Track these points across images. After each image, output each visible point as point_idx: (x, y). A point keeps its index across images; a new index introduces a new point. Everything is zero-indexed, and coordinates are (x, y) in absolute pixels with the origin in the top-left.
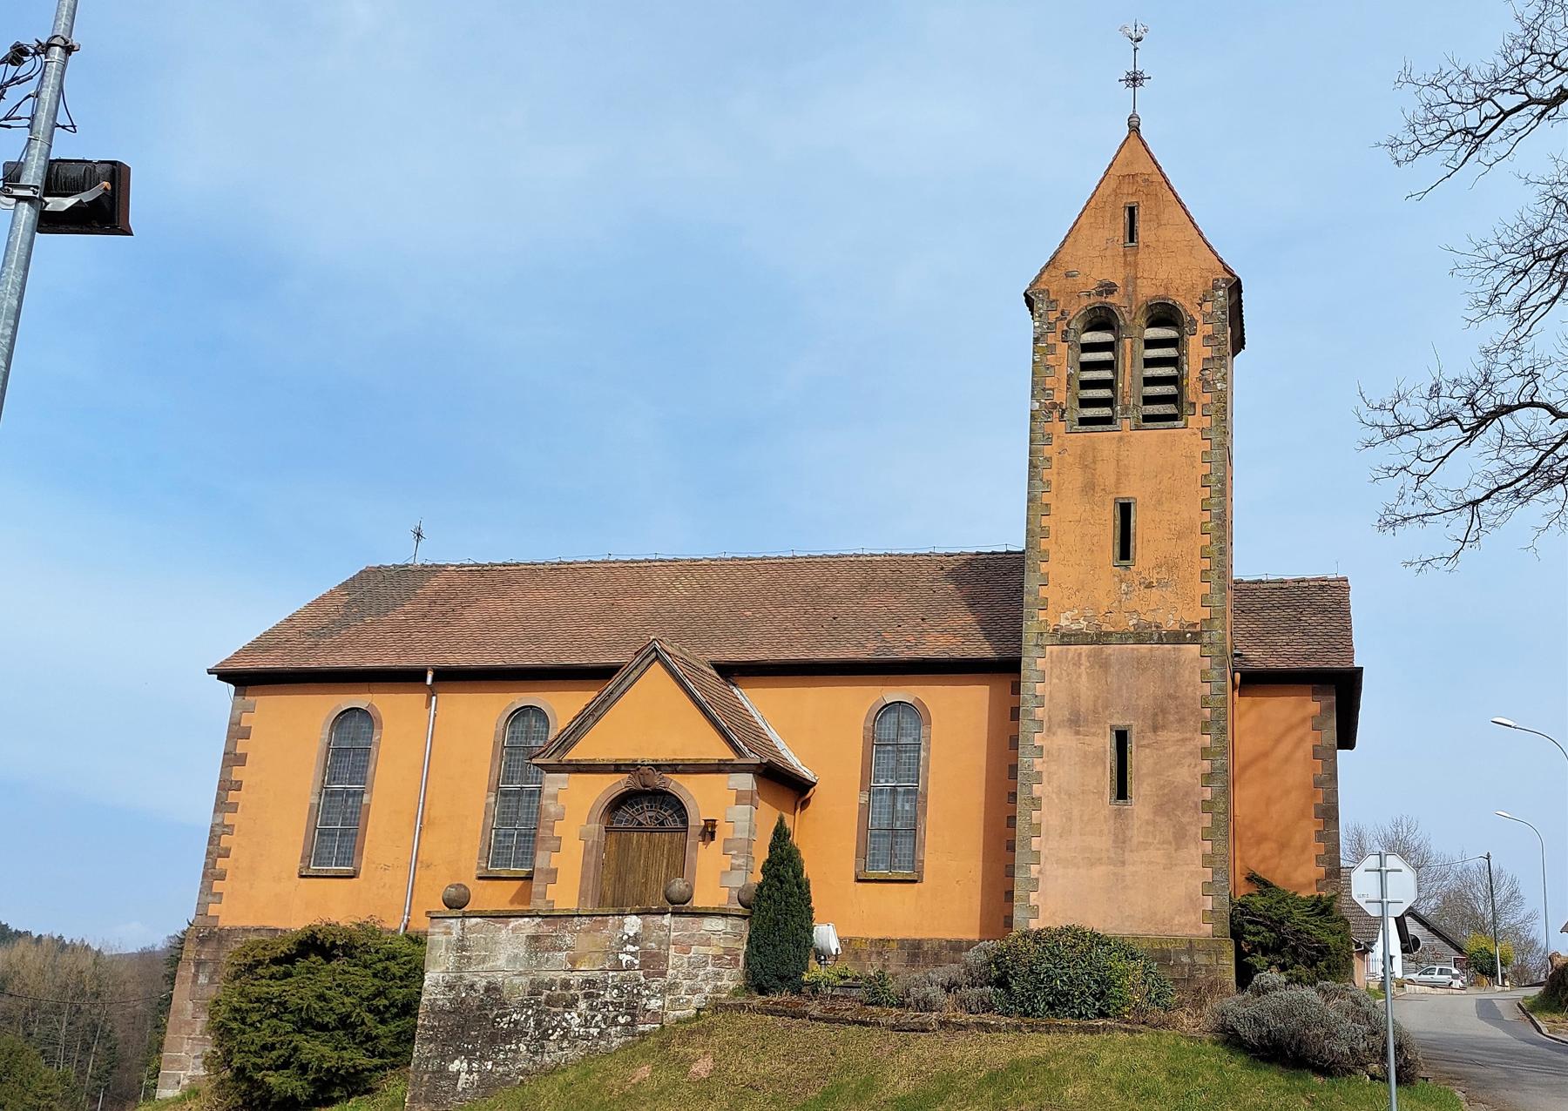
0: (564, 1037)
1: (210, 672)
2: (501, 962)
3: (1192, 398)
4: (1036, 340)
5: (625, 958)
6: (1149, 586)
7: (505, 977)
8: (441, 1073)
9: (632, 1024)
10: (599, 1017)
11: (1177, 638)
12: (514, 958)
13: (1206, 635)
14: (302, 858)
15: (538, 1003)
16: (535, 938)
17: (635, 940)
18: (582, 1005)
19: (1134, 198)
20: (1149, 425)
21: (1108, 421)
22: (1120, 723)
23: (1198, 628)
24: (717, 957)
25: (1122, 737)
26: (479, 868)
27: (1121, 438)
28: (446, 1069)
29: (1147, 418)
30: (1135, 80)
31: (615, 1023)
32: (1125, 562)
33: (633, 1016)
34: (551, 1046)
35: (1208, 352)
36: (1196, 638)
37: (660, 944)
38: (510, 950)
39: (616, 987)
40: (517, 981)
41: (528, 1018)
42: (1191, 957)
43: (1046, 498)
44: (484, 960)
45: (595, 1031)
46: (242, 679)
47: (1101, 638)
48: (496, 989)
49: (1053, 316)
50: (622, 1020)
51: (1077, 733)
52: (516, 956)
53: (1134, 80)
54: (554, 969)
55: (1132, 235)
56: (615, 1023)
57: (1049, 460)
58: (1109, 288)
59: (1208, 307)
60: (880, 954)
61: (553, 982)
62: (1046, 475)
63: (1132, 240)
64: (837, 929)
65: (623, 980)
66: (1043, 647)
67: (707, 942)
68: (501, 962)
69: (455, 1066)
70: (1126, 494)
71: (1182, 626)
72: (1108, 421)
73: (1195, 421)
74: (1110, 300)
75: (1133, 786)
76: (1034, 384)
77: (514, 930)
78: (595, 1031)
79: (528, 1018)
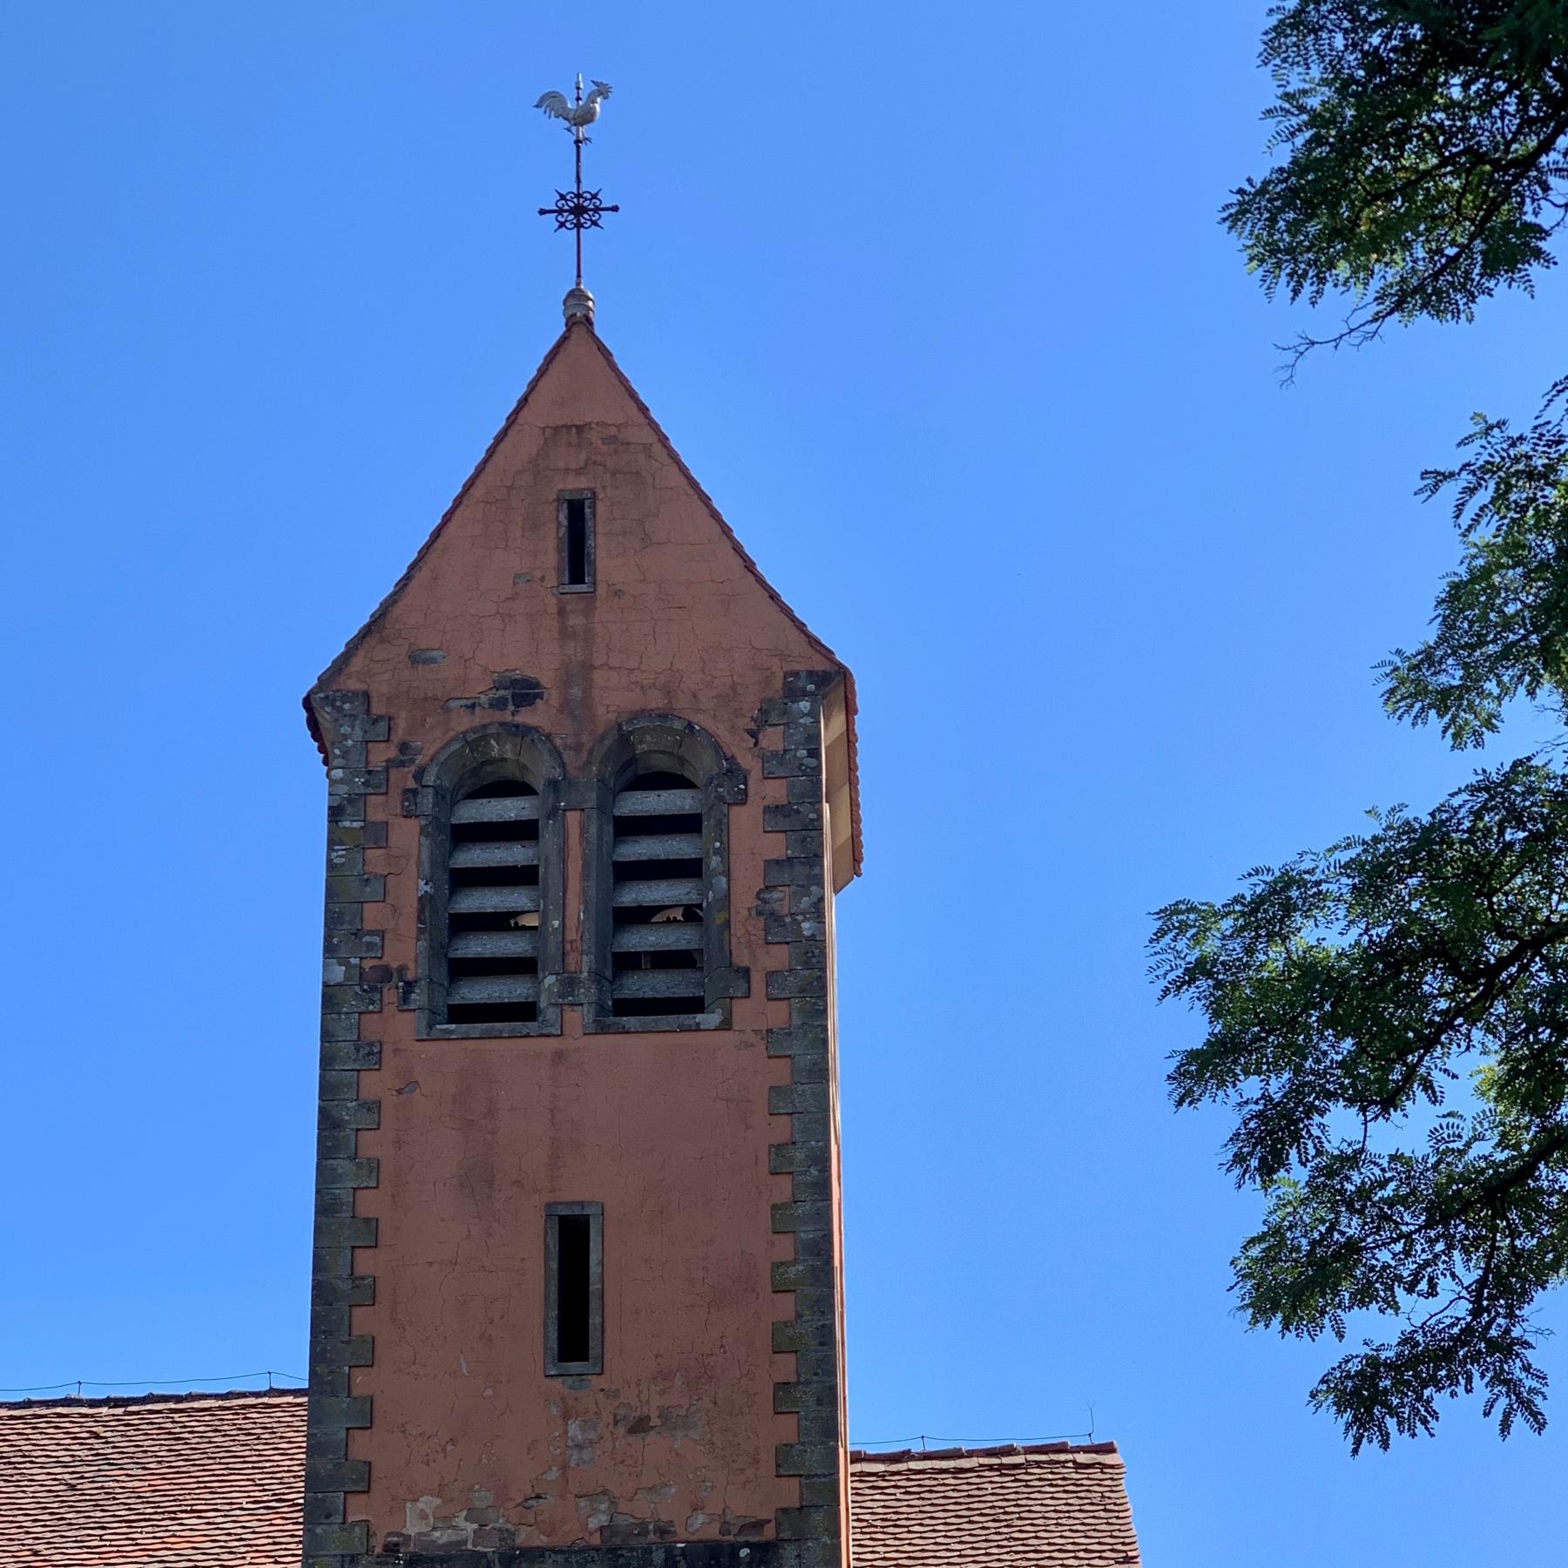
4: (335, 813)
6: (640, 1426)
19: (579, 480)
20: (631, 1022)
21: (525, 1011)
23: (769, 1533)
27: (559, 1056)
29: (626, 1007)
30: (579, 211)
32: (575, 1366)
49: (381, 755)
53: (578, 211)
55: (577, 564)
57: (374, 1107)
58: (524, 692)
59: (773, 739)
62: (372, 1146)
70: (576, 1191)
72: (525, 1011)
74: (526, 717)
76: (332, 921)
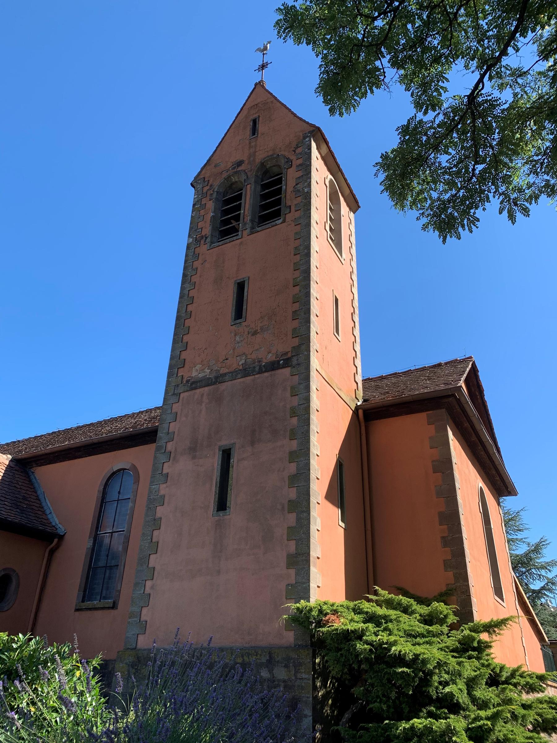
3: (289, 203)
6: (255, 333)
11: (273, 366)
13: (295, 359)
23: (289, 355)
27: (241, 243)
42: (271, 671)
43: (194, 279)
63: (254, 134)
75: (232, 499)
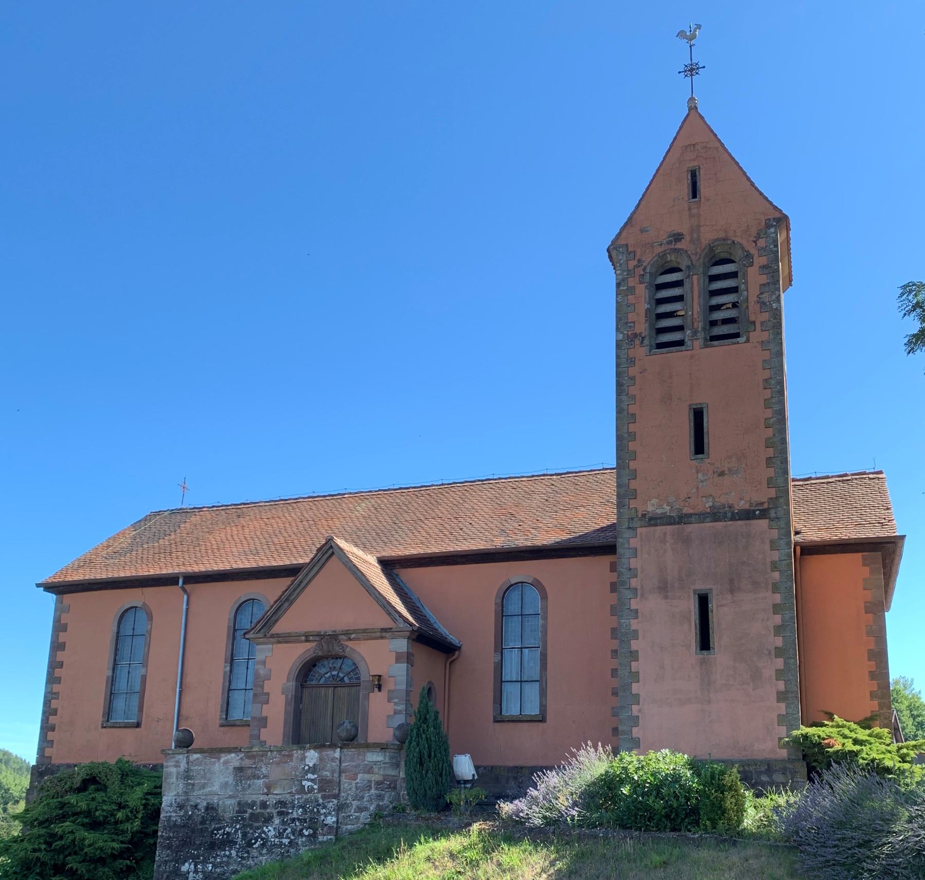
0: (263, 845)
1: (38, 585)
2: (216, 788)
4: (618, 285)
5: (307, 784)
6: (722, 474)
7: (219, 800)
8: (177, 872)
9: (314, 836)
10: (289, 830)
11: (747, 515)
12: (225, 785)
14: (103, 715)
15: (243, 819)
16: (239, 770)
17: (313, 770)
18: (277, 821)
21: (680, 343)
22: (701, 586)
23: (766, 506)
24: (378, 783)
25: (703, 601)
26: (221, 718)
27: (692, 357)
28: (179, 869)
30: (692, 70)
31: (301, 835)
32: (700, 456)
33: (315, 830)
34: (254, 853)
35: (764, 279)
36: (764, 514)
37: (333, 772)
38: (223, 780)
39: (301, 807)
40: (228, 802)
41: (236, 831)
42: (770, 777)
43: (632, 409)
44: (203, 786)
45: (286, 841)
46: (59, 589)
47: (682, 519)
48: (213, 808)
49: (632, 264)
50: (306, 833)
51: (666, 597)
52: (226, 783)
54: (255, 793)
56: (301, 835)
58: (678, 237)
60: (515, 778)
61: (254, 803)
62: (633, 391)
64: (473, 758)
65: (307, 801)
66: (634, 529)
67: (369, 770)
68: (216, 788)
69: (185, 868)
70: (698, 400)
71: (751, 505)
72: (680, 343)
73: (757, 335)
74: (679, 246)
77: (226, 763)
78: (286, 841)
79: (236, 831)
